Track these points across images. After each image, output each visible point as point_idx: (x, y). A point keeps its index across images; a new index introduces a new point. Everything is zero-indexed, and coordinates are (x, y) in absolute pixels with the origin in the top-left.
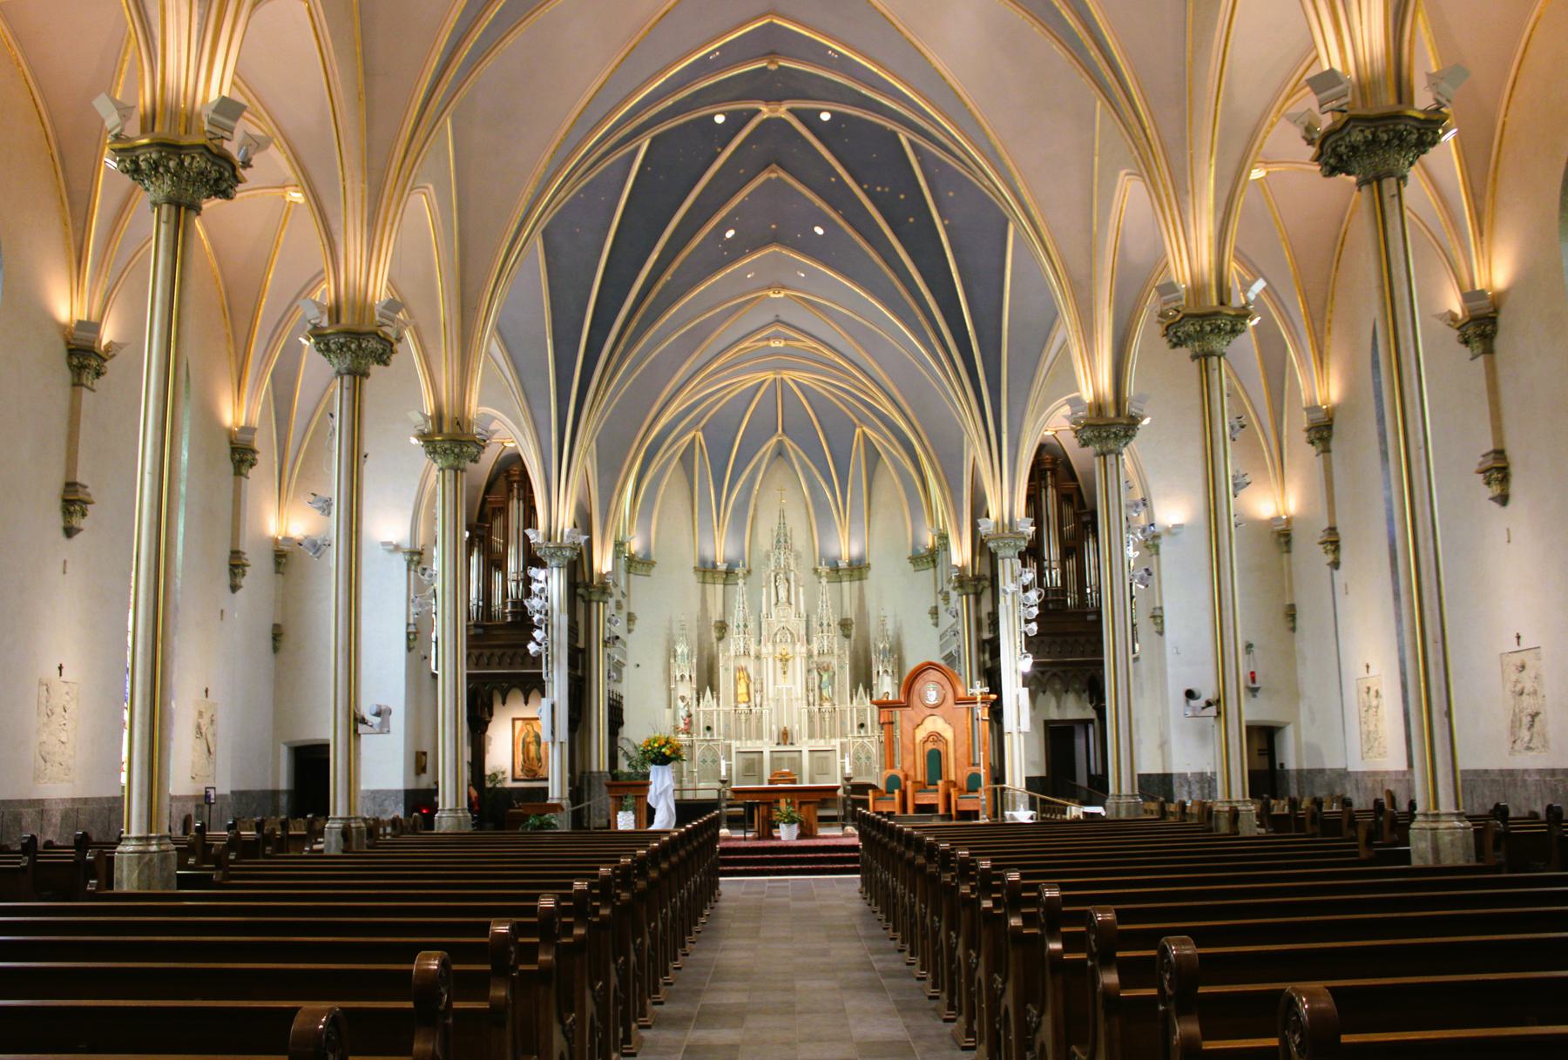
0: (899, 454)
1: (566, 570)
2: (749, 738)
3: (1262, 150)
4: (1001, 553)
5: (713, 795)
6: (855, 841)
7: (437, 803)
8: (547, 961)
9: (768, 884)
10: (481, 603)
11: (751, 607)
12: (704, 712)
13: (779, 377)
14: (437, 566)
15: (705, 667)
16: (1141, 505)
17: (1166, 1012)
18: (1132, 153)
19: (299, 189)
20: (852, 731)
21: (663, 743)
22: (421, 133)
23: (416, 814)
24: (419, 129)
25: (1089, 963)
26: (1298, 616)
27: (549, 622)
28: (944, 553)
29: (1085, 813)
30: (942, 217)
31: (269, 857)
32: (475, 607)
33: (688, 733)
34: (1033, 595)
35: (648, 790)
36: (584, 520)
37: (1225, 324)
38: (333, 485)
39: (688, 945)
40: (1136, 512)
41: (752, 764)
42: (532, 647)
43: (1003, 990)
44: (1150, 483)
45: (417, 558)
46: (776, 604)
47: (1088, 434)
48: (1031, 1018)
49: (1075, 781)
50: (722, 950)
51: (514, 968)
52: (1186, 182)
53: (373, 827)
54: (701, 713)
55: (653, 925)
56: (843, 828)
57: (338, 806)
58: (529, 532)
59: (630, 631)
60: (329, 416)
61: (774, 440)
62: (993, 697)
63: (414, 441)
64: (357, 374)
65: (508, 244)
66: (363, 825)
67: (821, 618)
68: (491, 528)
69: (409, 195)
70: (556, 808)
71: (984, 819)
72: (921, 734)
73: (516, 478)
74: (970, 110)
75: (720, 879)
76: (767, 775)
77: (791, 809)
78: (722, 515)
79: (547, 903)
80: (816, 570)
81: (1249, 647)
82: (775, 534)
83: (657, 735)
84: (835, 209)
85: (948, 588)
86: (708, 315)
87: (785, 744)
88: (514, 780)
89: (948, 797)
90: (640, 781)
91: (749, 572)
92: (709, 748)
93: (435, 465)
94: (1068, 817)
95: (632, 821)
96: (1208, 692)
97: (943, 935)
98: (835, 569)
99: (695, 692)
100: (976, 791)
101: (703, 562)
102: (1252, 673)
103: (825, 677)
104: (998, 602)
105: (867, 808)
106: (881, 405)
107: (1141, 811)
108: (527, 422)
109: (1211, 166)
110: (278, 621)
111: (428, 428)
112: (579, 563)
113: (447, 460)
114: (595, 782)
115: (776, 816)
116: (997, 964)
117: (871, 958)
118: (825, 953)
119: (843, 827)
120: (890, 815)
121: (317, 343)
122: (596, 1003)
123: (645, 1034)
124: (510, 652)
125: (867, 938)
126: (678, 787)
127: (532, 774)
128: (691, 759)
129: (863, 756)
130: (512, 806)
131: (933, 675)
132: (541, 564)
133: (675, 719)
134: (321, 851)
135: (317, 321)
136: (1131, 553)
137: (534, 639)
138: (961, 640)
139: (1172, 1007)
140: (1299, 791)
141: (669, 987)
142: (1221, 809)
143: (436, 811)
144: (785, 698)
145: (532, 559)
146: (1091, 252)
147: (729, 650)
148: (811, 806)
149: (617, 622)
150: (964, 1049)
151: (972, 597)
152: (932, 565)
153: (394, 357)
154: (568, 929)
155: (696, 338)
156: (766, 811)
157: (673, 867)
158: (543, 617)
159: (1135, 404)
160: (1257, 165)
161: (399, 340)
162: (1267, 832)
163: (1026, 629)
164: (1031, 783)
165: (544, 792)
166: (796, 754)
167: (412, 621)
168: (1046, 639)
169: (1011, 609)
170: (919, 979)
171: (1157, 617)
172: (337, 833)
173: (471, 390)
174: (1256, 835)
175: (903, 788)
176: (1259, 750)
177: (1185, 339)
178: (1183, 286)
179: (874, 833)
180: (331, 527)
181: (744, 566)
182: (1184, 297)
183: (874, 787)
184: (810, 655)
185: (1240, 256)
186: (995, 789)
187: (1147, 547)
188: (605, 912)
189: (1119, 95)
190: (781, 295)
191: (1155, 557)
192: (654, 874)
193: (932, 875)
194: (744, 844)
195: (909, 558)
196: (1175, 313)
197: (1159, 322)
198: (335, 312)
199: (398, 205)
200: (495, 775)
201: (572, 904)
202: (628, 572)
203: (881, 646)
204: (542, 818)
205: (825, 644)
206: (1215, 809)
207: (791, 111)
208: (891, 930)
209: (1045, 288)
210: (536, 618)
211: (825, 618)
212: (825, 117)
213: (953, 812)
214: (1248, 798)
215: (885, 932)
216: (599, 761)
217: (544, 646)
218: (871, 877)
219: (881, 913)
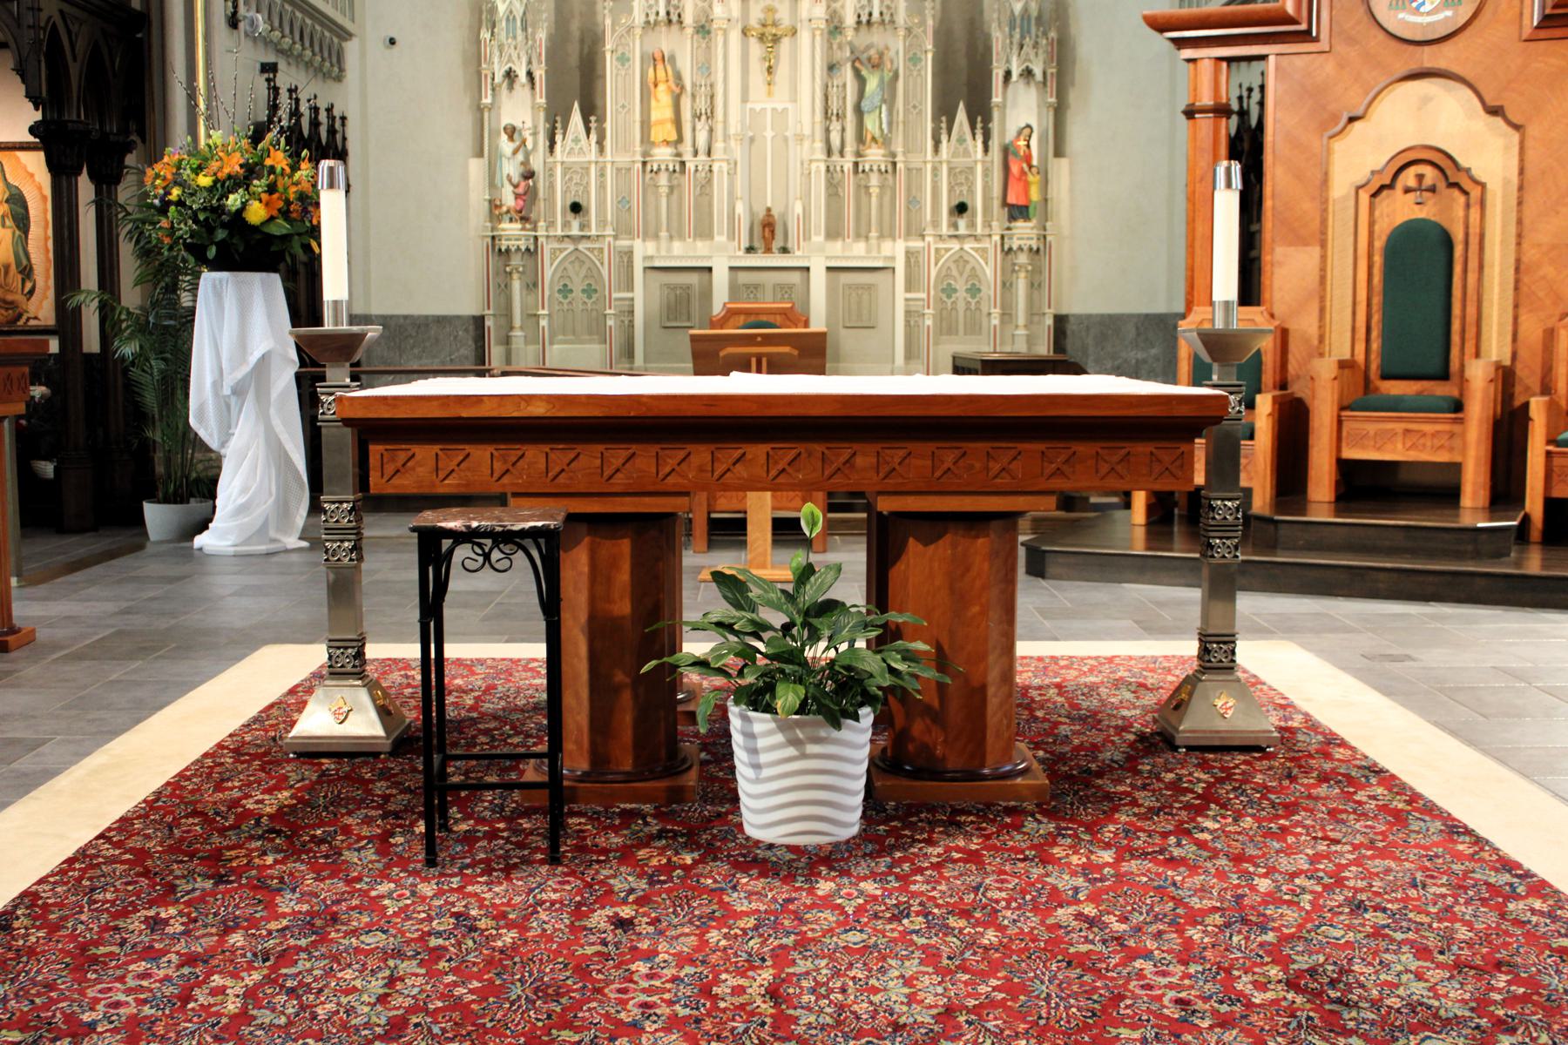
20: (936, 223)
87: (768, 250)
99: (542, 115)
103: (872, 84)
129: (961, 286)
144: (769, 134)
166: (795, 278)
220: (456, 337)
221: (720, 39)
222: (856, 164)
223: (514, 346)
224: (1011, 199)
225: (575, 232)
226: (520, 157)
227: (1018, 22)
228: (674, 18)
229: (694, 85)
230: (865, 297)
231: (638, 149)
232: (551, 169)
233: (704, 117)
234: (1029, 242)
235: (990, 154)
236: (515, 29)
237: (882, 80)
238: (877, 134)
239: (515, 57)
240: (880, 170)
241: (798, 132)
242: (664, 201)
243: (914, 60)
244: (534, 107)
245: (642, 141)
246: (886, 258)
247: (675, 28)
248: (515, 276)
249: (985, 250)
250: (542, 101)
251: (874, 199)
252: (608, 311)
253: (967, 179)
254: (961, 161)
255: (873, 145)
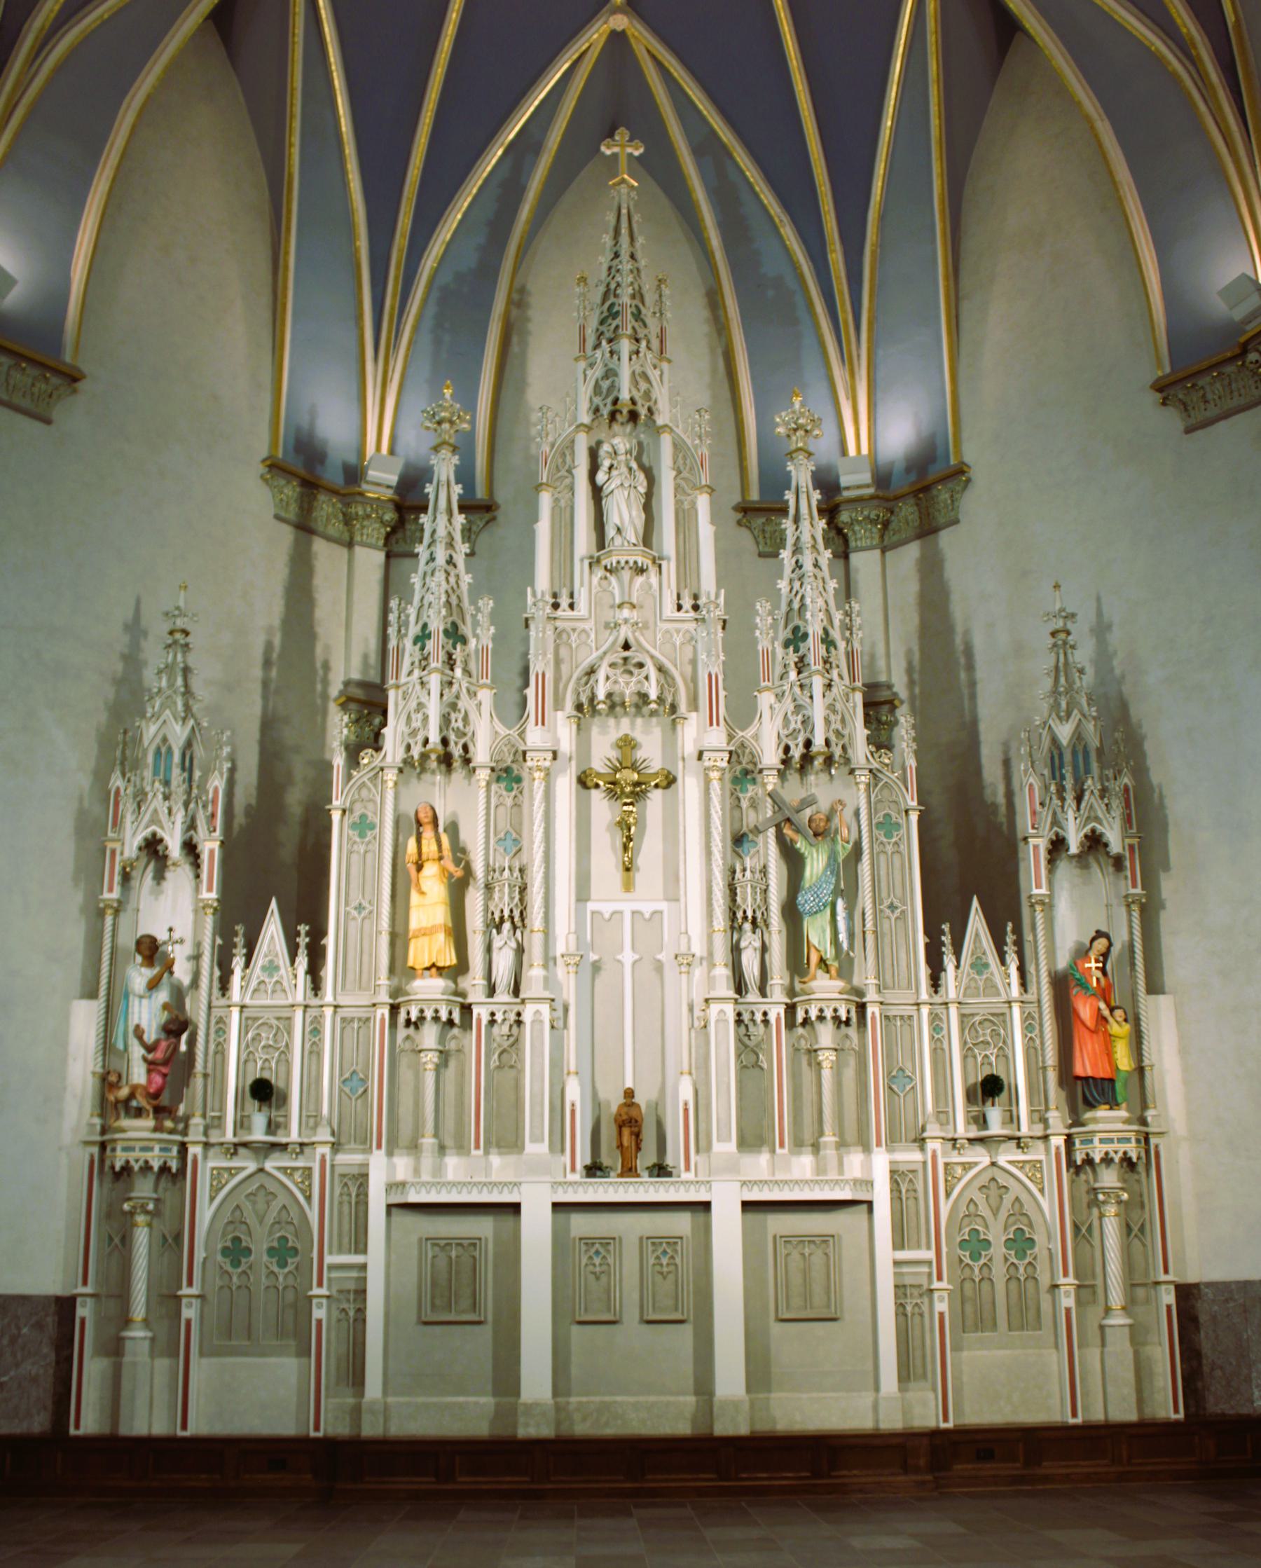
20: (944, 1116)
61: (595, 36)
87: (629, 1170)
99: (209, 921)
103: (816, 864)
129: (997, 1235)
144: (628, 957)
166: (682, 1223)
205: (818, 712)
220: (13, 1340)
221: (538, 788)
222: (791, 1009)
223: (127, 1359)
224: (1083, 1067)
225: (258, 1134)
226: (163, 996)
227: (1068, 757)
228: (457, 751)
229: (489, 869)
230: (817, 1259)
231: (383, 980)
232: (220, 1020)
233: (507, 926)
234: (1122, 1147)
235: (942, 990)
236: (168, 769)
237: (833, 856)
238: (829, 953)
239: (163, 814)
240: (836, 1019)
241: (683, 949)
242: (429, 1079)
243: (887, 826)
244: (200, 908)
245: (392, 970)
246: (856, 1182)
247: (459, 774)
248: (140, 1219)
249: (1037, 1165)
250: (211, 896)
251: (827, 1074)
252: (316, 1291)
253: (995, 1033)
254: (982, 1005)
255: (820, 973)
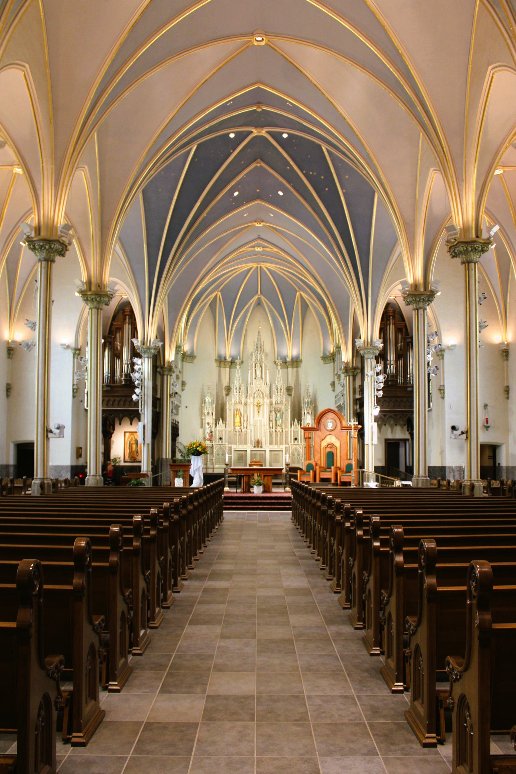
0: (317, 305)
1: (152, 359)
2: (240, 443)
3: (501, 160)
4: (366, 356)
5: (222, 471)
6: (290, 495)
7: (87, 473)
8: (137, 545)
9: (247, 514)
10: (109, 375)
11: (243, 380)
12: (219, 431)
13: (259, 266)
14: (88, 356)
15: (219, 409)
16: (435, 335)
17: (422, 573)
18: (436, 160)
19: (20, 167)
20: (291, 442)
21: (198, 445)
22: (82, 141)
23: (76, 477)
24: (81, 138)
25: (390, 551)
26: (510, 392)
27: (143, 385)
28: (338, 355)
29: (402, 484)
30: (342, 189)
31: (5, 496)
32: (106, 377)
33: (210, 441)
34: (381, 378)
35: (190, 468)
36: (161, 335)
37: (479, 247)
38: (37, 316)
39: (207, 543)
40: (432, 338)
41: (241, 456)
42: (134, 397)
43: (353, 565)
44: (440, 324)
45: (78, 352)
46: (255, 378)
47: (410, 299)
48: (365, 578)
49: (399, 469)
50: (223, 545)
51: (121, 548)
52: (462, 176)
53: (55, 483)
54: (217, 431)
55: (189, 531)
56: (285, 488)
57: (38, 472)
58: (134, 340)
59: (183, 390)
60: (35, 281)
62: (360, 426)
63: (77, 294)
64: (49, 261)
65: (124, 197)
66: (50, 482)
67: (277, 386)
68: (115, 337)
69: (75, 171)
70: (145, 475)
71: (353, 486)
72: (324, 444)
73: (128, 313)
74: (357, 135)
75: (224, 511)
76: (249, 462)
77: (259, 478)
78: (229, 334)
79: (138, 518)
80: (275, 362)
81: (486, 406)
82: (256, 344)
83: (195, 441)
84: (289, 183)
85: (340, 373)
86: (224, 234)
87: (258, 447)
88: (125, 462)
89: (336, 475)
90: (186, 464)
91: (242, 362)
92: (221, 448)
93: (87, 306)
94: (394, 486)
95: (182, 483)
96: (462, 427)
97: (328, 539)
98: (285, 362)
99: (214, 421)
100: (350, 472)
101: (220, 357)
102: (487, 419)
103: (278, 415)
104: (364, 380)
105: (297, 479)
106: (310, 281)
107: (428, 484)
108: (133, 285)
109: (475, 168)
110: (9, 382)
111: (84, 288)
112: (158, 356)
113: (93, 304)
114: (164, 463)
115: (252, 482)
116: (351, 553)
117: (295, 550)
118: (272, 547)
119: (285, 488)
120: (308, 483)
121: (29, 245)
122: (161, 567)
123: (185, 583)
124: (124, 399)
125: (295, 541)
126: (205, 466)
127: (133, 459)
128: (212, 453)
129: (296, 454)
130: (124, 475)
131: (331, 415)
132: (139, 356)
133: (204, 434)
134: (30, 494)
135: (29, 234)
136: (430, 358)
137: (135, 393)
138: (345, 398)
139: (424, 571)
140: (507, 476)
141: (197, 562)
142: (466, 484)
143: (86, 476)
145: (135, 354)
146: (415, 208)
147: (231, 401)
148: (269, 477)
149: (176, 385)
150: (335, 593)
151: (351, 378)
152: (332, 361)
153: (67, 253)
154: (147, 532)
155: (218, 246)
156: (247, 479)
157: (200, 505)
158: (140, 382)
159: (434, 285)
160: (498, 167)
161: (70, 244)
162: (489, 495)
163: (377, 394)
164: (377, 469)
165: (139, 467)
166: (263, 452)
167: (75, 383)
168: (387, 399)
169: (370, 384)
170: (316, 560)
171: (441, 390)
172: (38, 485)
173: (105, 269)
174: (482, 496)
175: (314, 470)
176: (489, 456)
177: (459, 254)
178: (459, 227)
179: (298, 491)
180: (36, 336)
181: (240, 359)
182: (459, 233)
183: (300, 469)
184: (271, 404)
185: (488, 212)
186: (360, 471)
187: (438, 355)
188: (166, 524)
189: (431, 130)
190: (261, 225)
191: (441, 361)
192: (190, 507)
193: (324, 510)
194: (236, 495)
195: (321, 357)
196: (454, 241)
197: (446, 245)
198: (38, 230)
199: (70, 176)
200: (115, 459)
201: (150, 520)
202: (183, 361)
203: (306, 400)
204: (138, 480)
205: (279, 398)
206: (463, 484)
207: (267, 132)
208: (305, 537)
209: (391, 225)
210: (137, 383)
211: (279, 386)
212: (285, 136)
213: (339, 482)
214: (479, 479)
215: (302, 538)
216: (166, 453)
217: (140, 396)
218: (297, 512)
219: (301, 529)
